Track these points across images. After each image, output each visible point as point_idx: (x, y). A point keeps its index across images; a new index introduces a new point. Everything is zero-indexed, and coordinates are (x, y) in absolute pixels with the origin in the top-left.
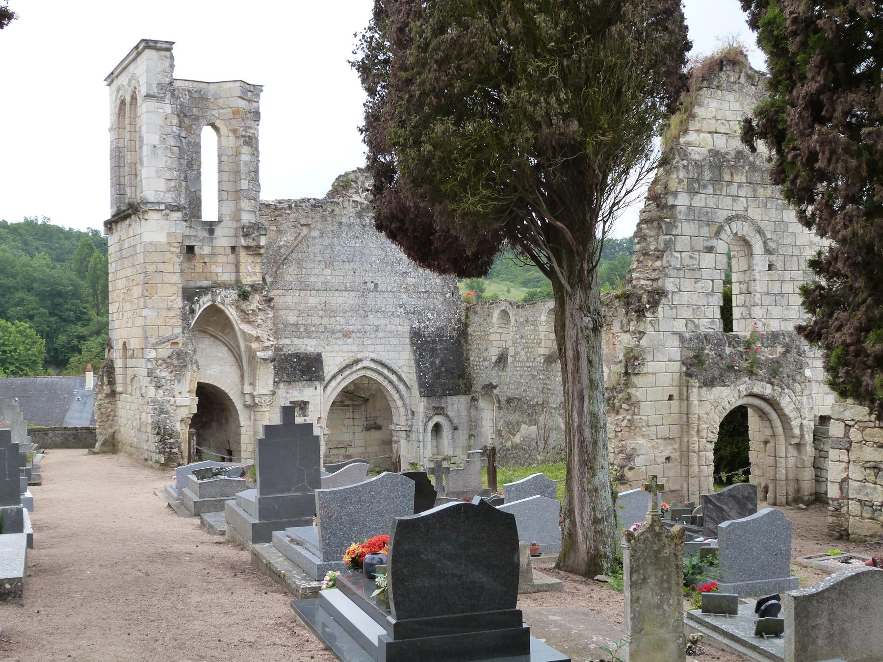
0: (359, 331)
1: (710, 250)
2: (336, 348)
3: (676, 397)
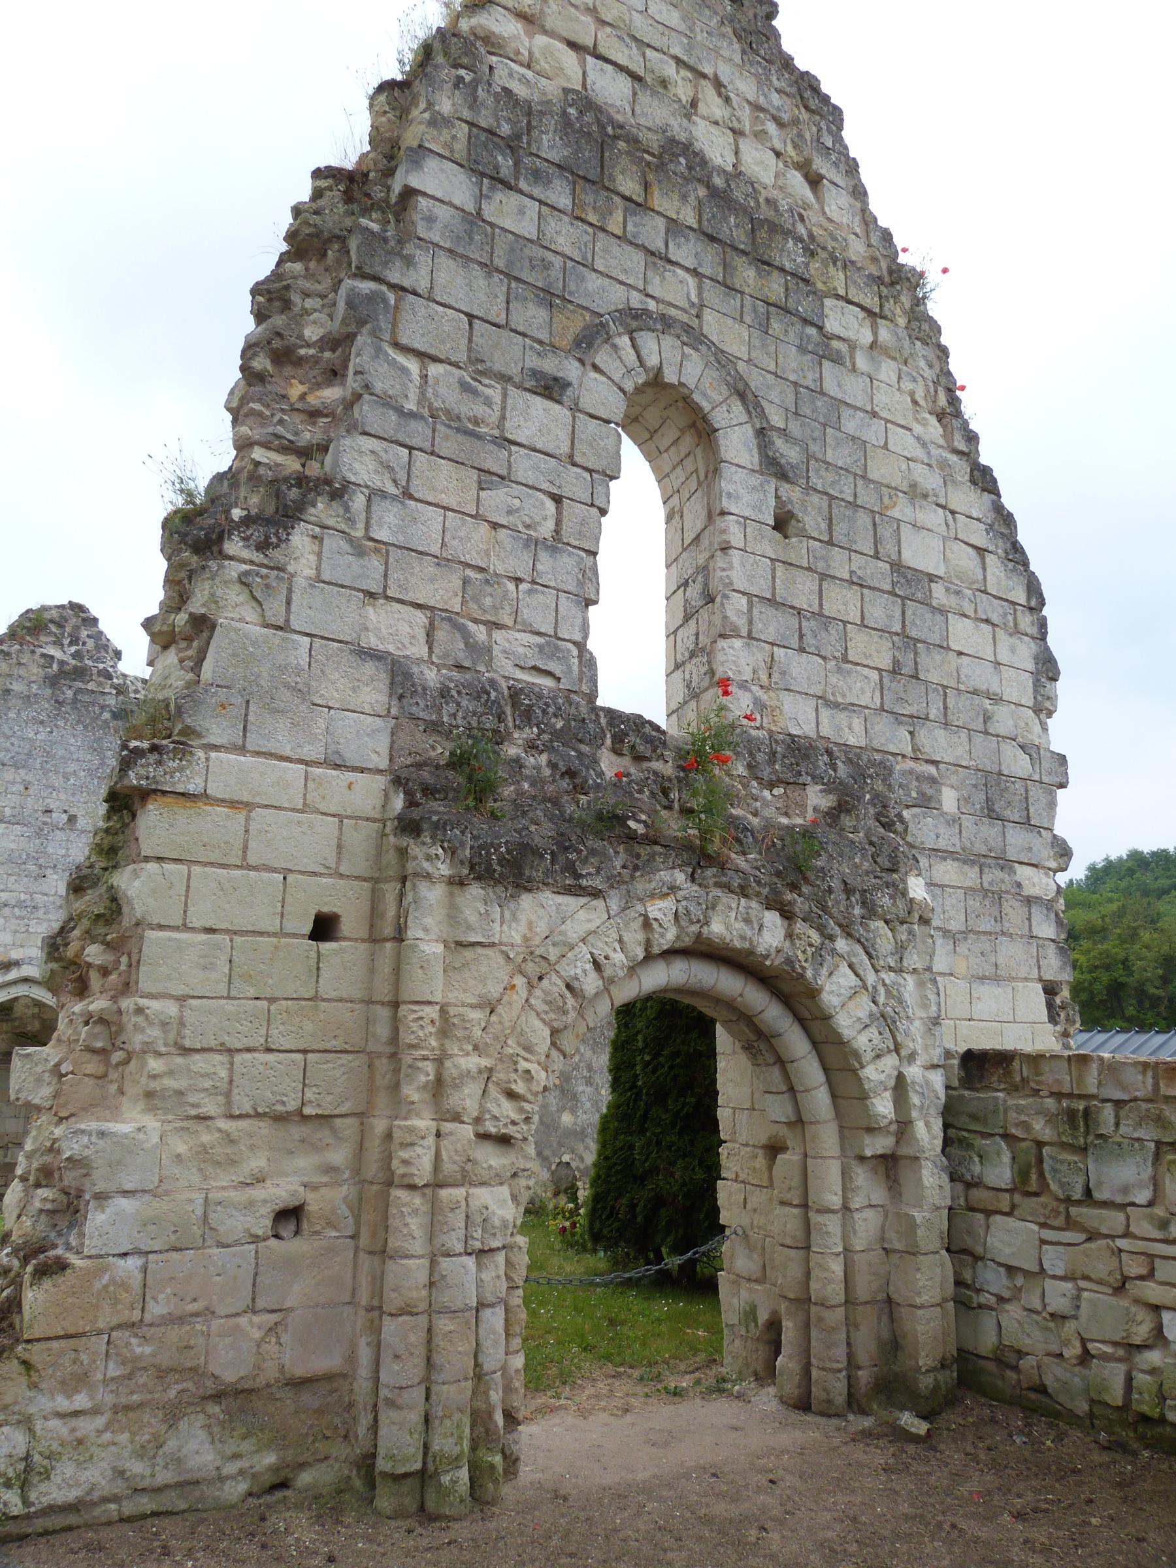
0: (20, 904)
1: (551, 388)
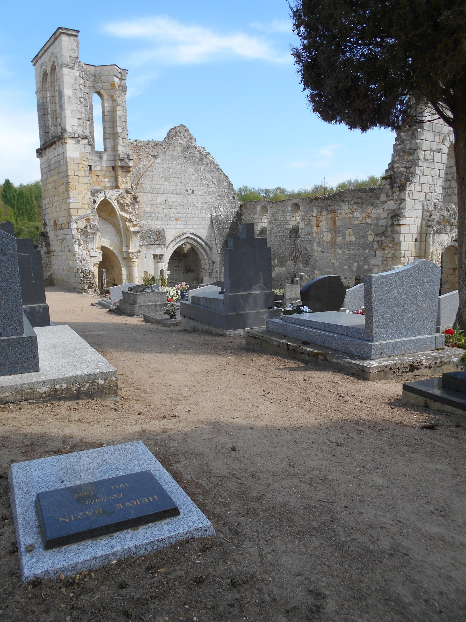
2: (172, 226)
3: (418, 240)
